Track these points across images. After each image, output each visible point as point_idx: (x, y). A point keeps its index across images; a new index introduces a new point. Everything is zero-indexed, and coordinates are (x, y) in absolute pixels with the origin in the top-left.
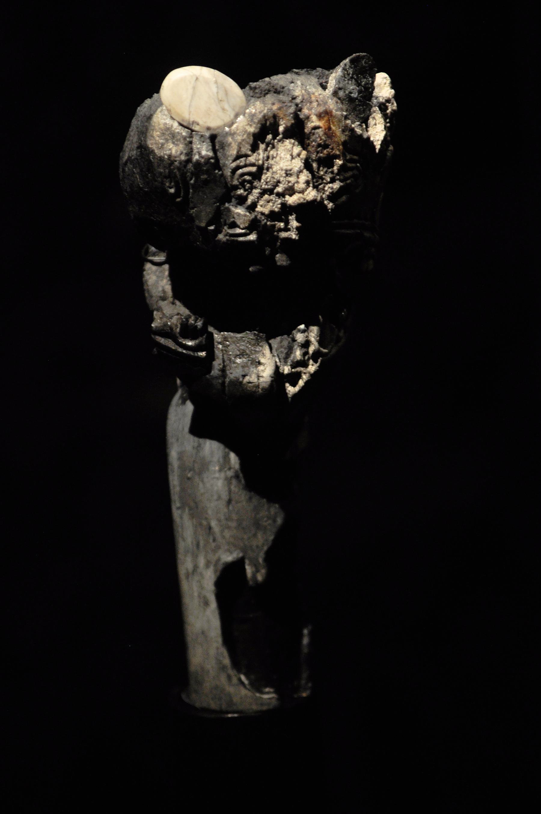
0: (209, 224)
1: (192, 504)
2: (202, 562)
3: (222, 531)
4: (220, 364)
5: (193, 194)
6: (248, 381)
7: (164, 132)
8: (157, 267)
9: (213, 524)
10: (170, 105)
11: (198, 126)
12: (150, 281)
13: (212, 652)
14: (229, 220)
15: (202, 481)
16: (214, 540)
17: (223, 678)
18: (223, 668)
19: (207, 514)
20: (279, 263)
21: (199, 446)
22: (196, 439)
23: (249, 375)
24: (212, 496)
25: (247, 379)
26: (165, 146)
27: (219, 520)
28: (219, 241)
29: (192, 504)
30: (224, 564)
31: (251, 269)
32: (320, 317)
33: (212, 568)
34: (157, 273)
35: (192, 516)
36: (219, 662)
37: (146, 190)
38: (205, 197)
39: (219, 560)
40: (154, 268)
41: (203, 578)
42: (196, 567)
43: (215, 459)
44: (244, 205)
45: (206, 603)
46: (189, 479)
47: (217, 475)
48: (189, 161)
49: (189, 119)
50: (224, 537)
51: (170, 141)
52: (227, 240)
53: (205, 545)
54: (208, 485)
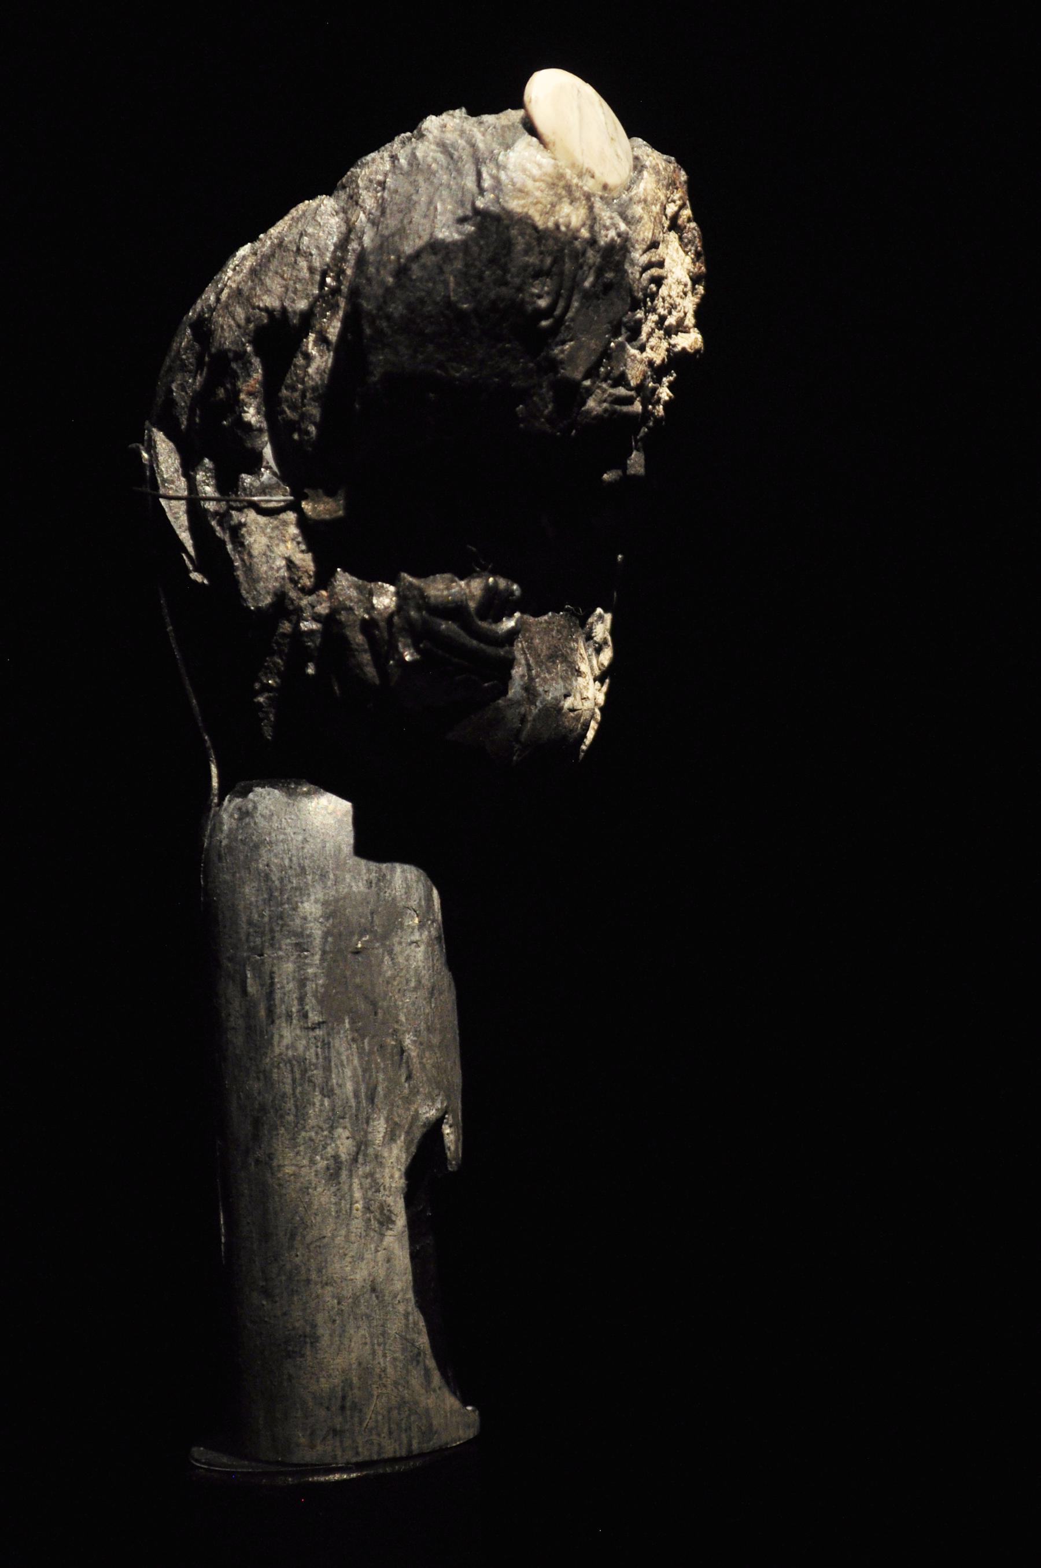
0: (585, 378)
1: (362, 1006)
2: (380, 1127)
3: (421, 1057)
4: (523, 676)
5: (578, 310)
6: (571, 707)
7: (556, 181)
8: (268, 518)
9: (408, 1041)
10: (554, 133)
11: (592, 179)
12: (256, 546)
13: (395, 1327)
14: (618, 369)
15: (390, 952)
16: (409, 1078)
17: (416, 1381)
18: (417, 1357)
19: (397, 1022)
20: (634, 469)
21: (382, 878)
22: (373, 865)
23: (573, 694)
24: (408, 981)
25: (567, 704)
26: (557, 208)
27: (417, 1033)
28: (589, 412)
29: (362, 1006)
30: (424, 1125)
31: (605, 476)
32: (615, 594)
33: (401, 1141)
34: (269, 530)
35: (359, 1034)
36: (408, 1343)
37: (465, 306)
38: (596, 318)
39: (416, 1116)
40: (262, 520)
41: (381, 1165)
42: (362, 1145)
43: (413, 904)
44: (634, 343)
45: (386, 1220)
46: (357, 952)
47: (416, 937)
48: (593, 242)
49: (583, 164)
50: (423, 1067)
51: (565, 199)
52: (606, 410)
53: (389, 1092)
54: (401, 959)
